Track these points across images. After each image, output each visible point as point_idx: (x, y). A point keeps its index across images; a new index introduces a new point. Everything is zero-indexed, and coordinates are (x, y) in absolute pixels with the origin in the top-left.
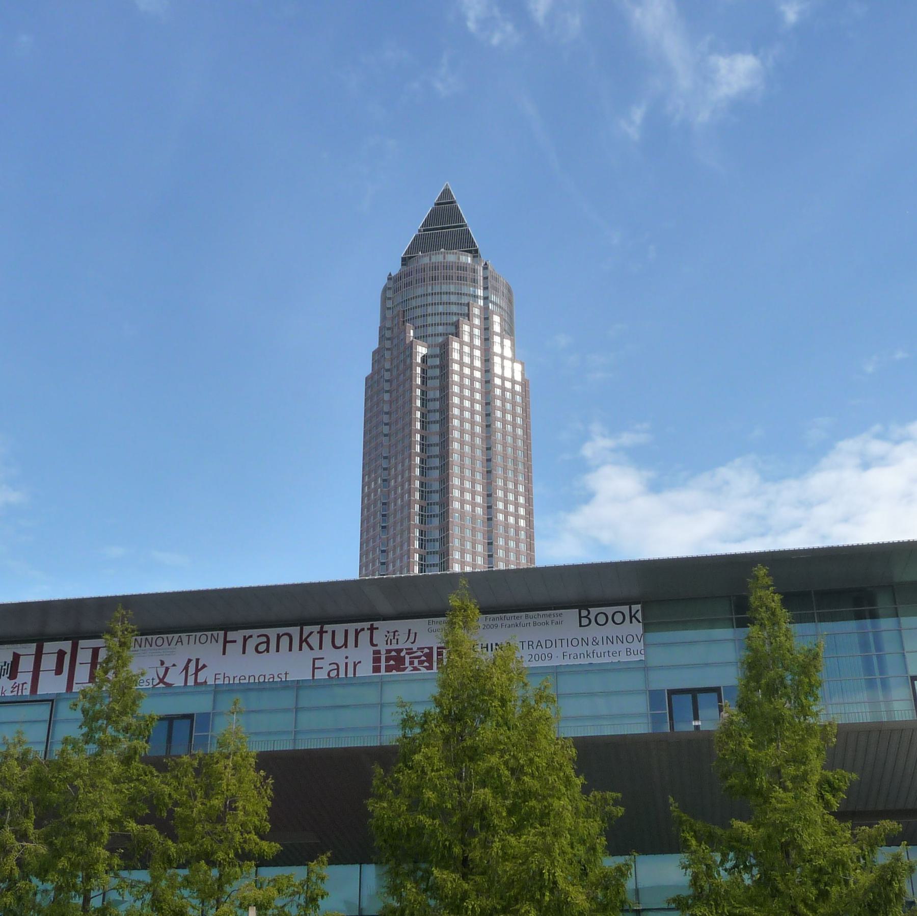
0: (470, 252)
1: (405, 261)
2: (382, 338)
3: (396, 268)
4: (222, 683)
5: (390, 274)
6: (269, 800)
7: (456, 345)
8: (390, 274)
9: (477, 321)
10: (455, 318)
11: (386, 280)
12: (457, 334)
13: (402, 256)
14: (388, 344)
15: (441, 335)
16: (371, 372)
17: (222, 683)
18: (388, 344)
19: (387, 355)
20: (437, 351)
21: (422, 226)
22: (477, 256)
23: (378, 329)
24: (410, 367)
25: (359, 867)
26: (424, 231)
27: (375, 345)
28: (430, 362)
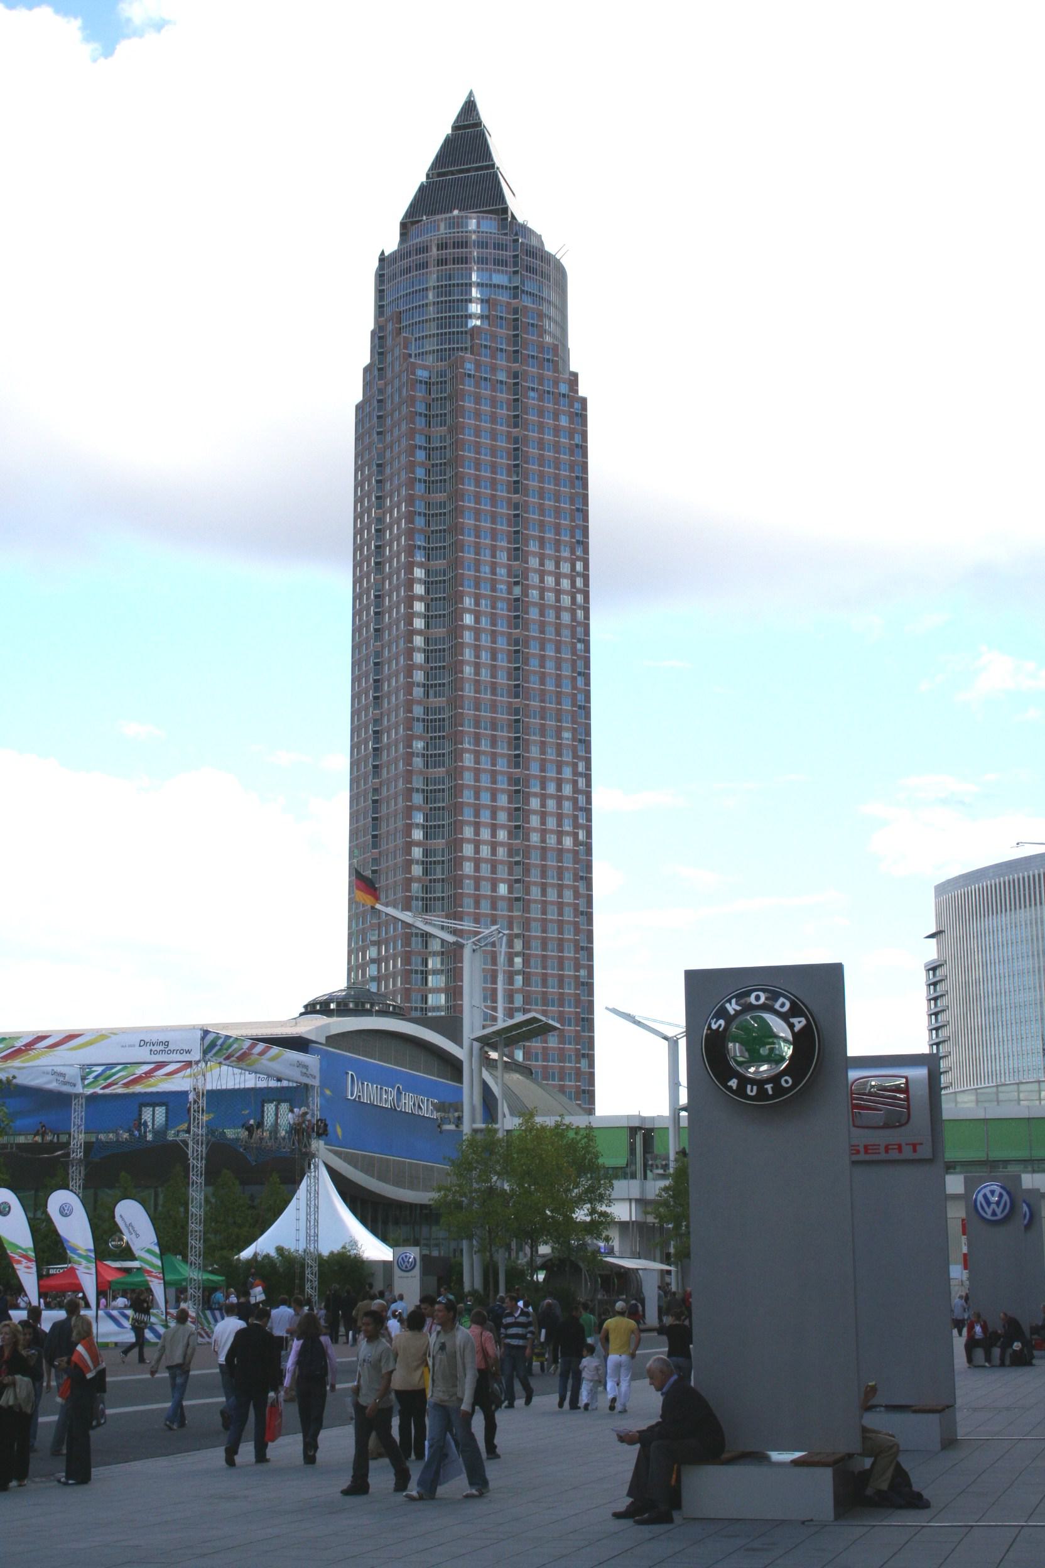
5: (383, 253)
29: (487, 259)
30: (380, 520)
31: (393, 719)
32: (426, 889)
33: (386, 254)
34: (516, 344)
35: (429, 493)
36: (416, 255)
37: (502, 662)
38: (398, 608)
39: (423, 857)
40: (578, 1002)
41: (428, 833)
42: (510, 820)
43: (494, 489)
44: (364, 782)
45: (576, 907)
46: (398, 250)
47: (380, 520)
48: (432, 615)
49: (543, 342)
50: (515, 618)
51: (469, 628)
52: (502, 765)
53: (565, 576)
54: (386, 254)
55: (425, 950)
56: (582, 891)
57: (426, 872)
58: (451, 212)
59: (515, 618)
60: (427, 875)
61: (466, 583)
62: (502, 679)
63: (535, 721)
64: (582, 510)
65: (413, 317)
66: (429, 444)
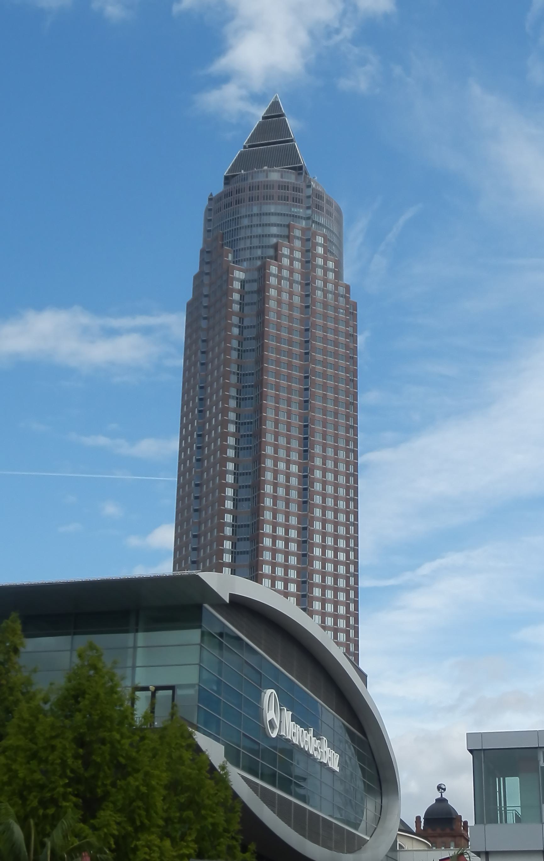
0: (294, 169)
1: (228, 180)
2: (203, 262)
3: (218, 187)
4: (520, 808)
5: (211, 195)
6: (339, 211)
7: (274, 269)
8: (211, 195)
9: (298, 244)
10: (274, 240)
11: (207, 202)
12: (276, 258)
13: (225, 174)
14: (207, 269)
15: (259, 258)
16: (191, 297)
17: (520, 808)
18: (207, 269)
19: (206, 280)
20: (256, 275)
21: (248, 142)
22: (302, 174)
23: (193, 278)
24: (228, 293)
25: (137, 668)
26: (250, 147)
27: (196, 269)
28: (247, 288)
29: (288, 197)
30: (202, 426)
31: (210, 511)
32: (240, 344)
33: (214, 195)
34: (307, 348)
35: (241, 382)
36: (236, 204)
37: (297, 288)
38: (211, 546)
39: (237, 419)
40: (347, 347)
41: (239, 401)
42: (298, 549)
43: (289, 405)
44: (185, 563)
45: (346, 310)
46: (223, 192)
47: (202, 426)
48: (241, 448)
49: (327, 278)
50: (305, 402)
51: (269, 509)
52: (295, 409)
53: (342, 537)
54: (214, 195)
55: (234, 564)
56: (351, 345)
57: (239, 380)
58: (262, 168)
59: (305, 402)
60: (236, 535)
61: (269, 398)
62: (297, 300)
63: (319, 416)
64: (353, 404)
65: (235, 235)
66: (236, 522)
